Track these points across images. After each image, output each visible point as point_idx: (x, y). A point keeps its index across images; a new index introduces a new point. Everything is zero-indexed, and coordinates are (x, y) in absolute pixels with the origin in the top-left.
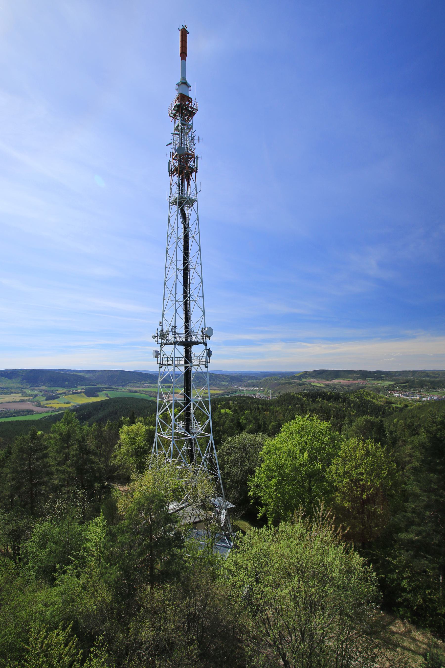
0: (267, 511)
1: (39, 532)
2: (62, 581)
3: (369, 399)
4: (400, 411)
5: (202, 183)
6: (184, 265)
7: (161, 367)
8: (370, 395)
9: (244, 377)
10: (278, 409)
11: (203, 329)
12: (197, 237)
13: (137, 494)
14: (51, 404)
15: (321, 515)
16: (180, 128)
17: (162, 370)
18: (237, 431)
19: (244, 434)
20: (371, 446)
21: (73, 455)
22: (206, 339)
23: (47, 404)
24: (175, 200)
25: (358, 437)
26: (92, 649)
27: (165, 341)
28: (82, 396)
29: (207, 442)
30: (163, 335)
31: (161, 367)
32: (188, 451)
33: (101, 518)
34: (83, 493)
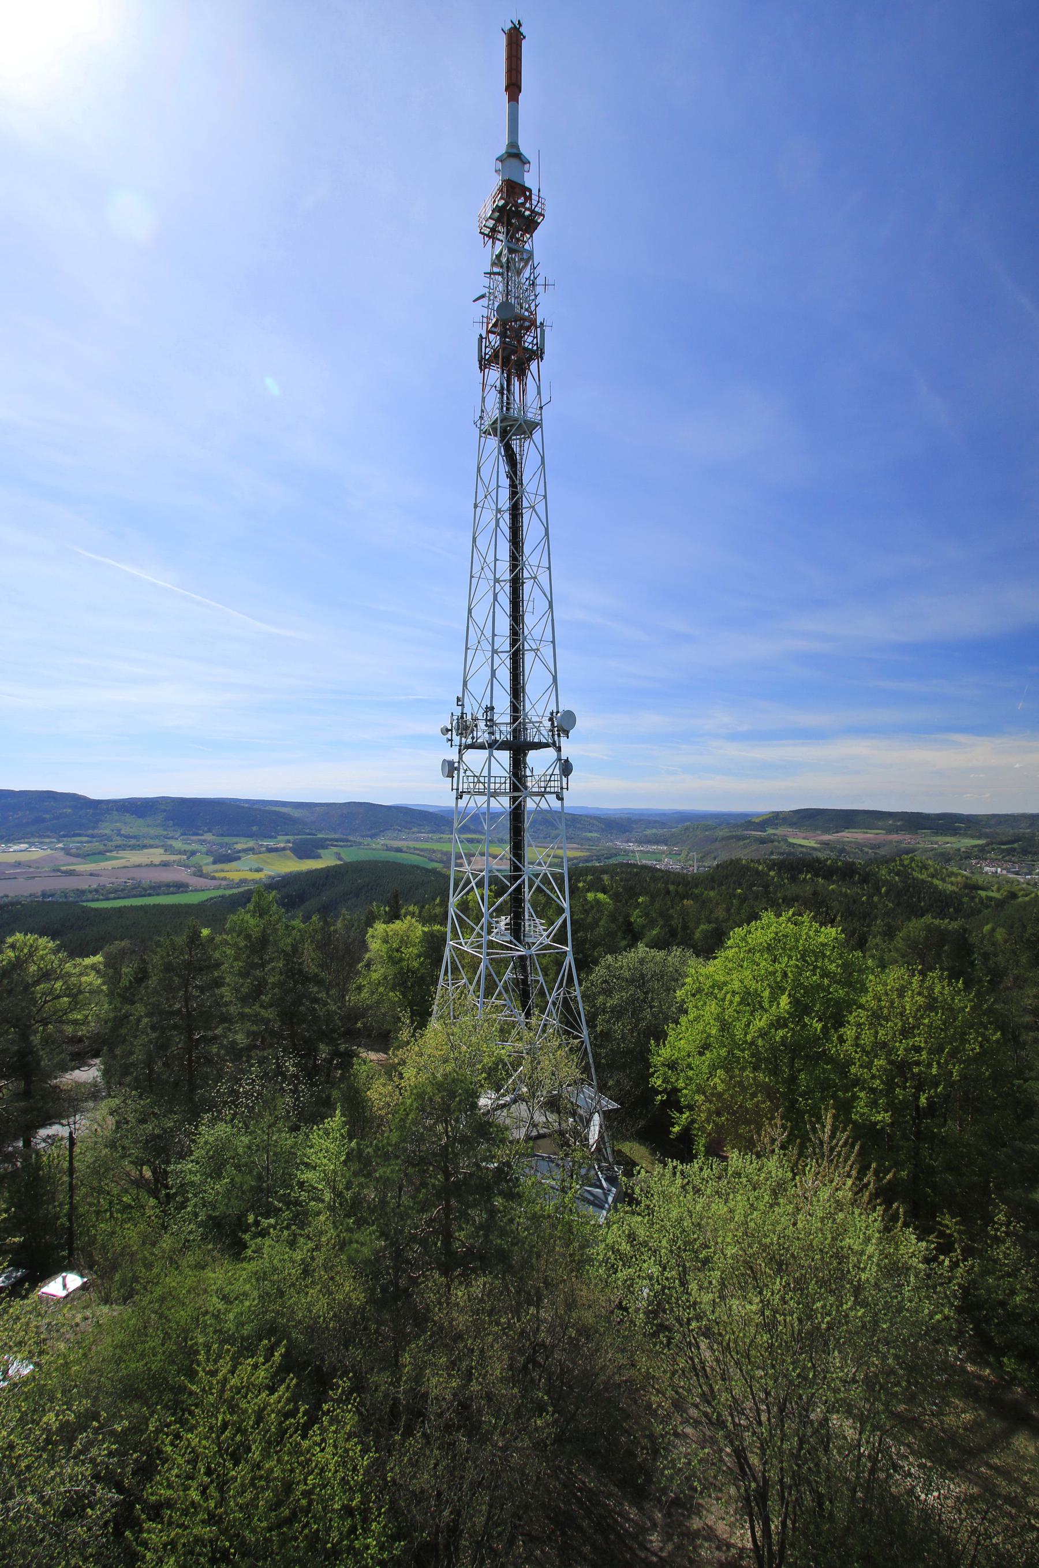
0: (693, 1121)
1: (206, 1143)
2: (258, 1250)
3: (923, 877)
4: (997, 906)
5: (554, 386)
6: (512, 571)
7: (460, 796)
8: (927, 869)
9: (636, 822)
10: (712, 894)
11: (552, 714)
12: (540, 508)
13: (409, 1072)
14: (223, 871)
15: (826, 1138)
16: (504, 260)
17: (462, 803)
18: (624, 943)
19: (641, 947)
20: (941, 988)
21: (273, 983)
22: (559, 736)
23: (217, 871)
24: (493, 423)
25: (909, 964)
26: (325, 1407)
27: (469, 741)
28: (287, 857)
29: (560, 964)
30: (463, 727)
31: (460, 796)
32: (516, 982)
33: (336, 1121)
34: (295, 1065)
